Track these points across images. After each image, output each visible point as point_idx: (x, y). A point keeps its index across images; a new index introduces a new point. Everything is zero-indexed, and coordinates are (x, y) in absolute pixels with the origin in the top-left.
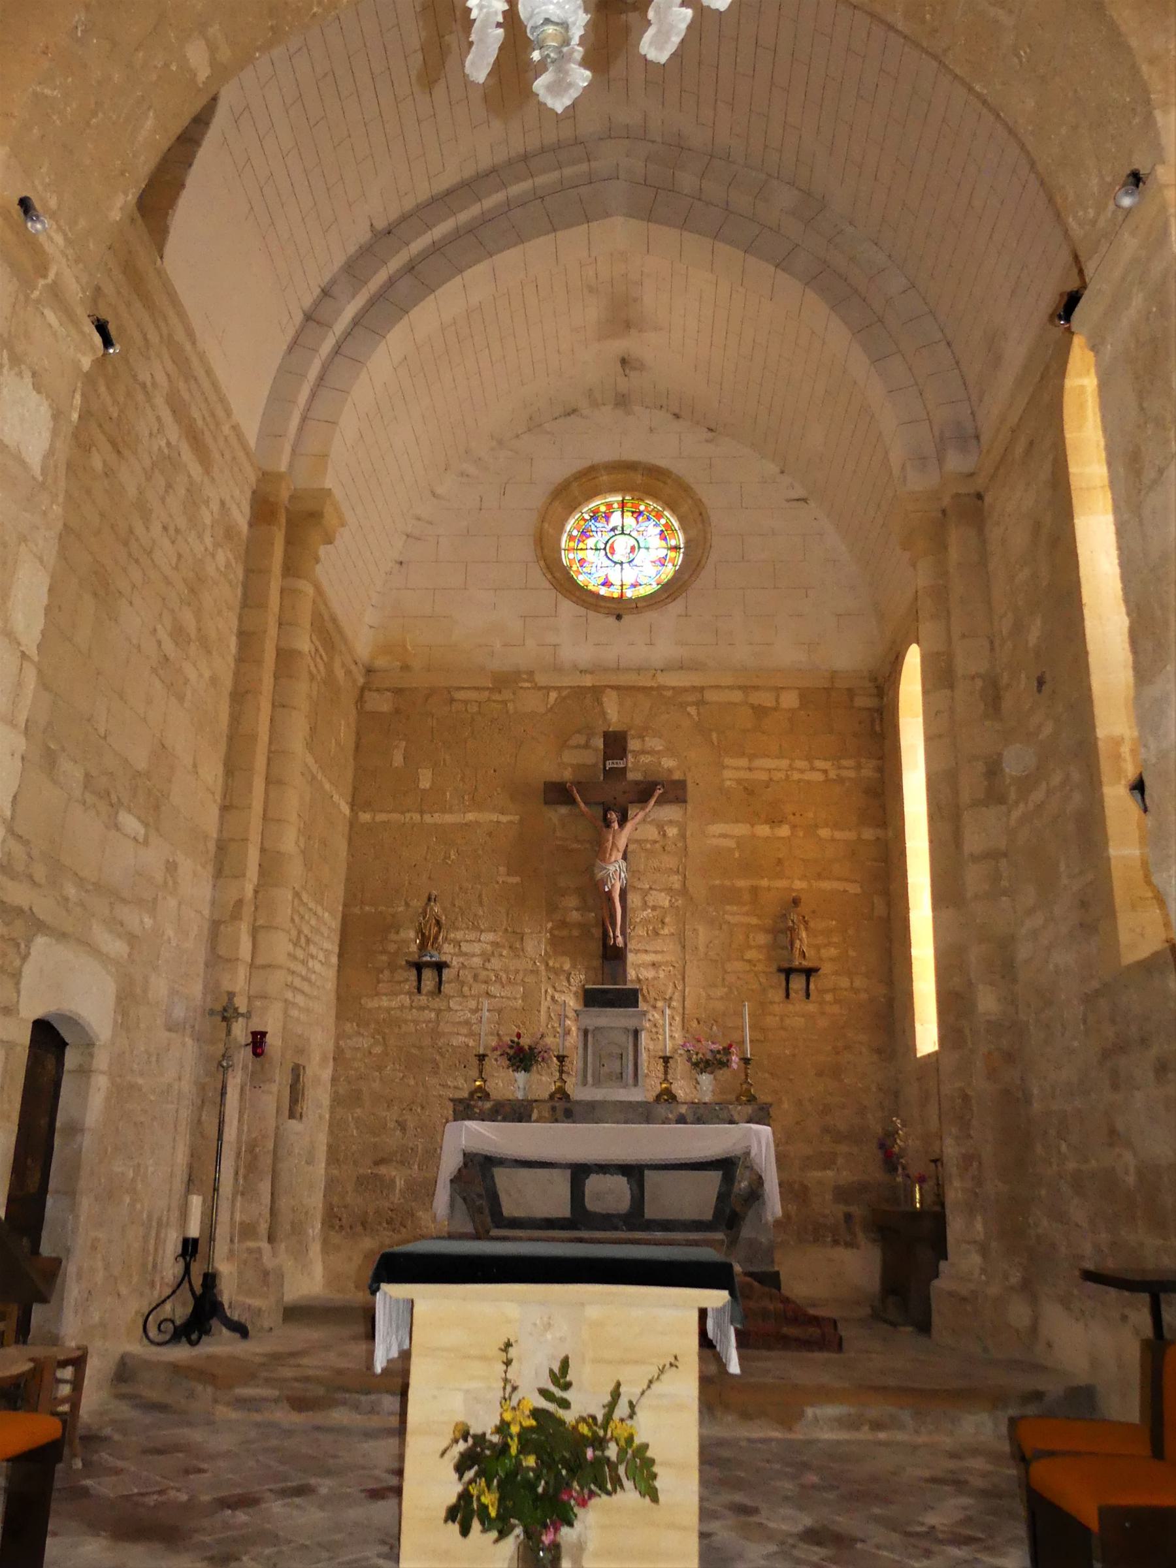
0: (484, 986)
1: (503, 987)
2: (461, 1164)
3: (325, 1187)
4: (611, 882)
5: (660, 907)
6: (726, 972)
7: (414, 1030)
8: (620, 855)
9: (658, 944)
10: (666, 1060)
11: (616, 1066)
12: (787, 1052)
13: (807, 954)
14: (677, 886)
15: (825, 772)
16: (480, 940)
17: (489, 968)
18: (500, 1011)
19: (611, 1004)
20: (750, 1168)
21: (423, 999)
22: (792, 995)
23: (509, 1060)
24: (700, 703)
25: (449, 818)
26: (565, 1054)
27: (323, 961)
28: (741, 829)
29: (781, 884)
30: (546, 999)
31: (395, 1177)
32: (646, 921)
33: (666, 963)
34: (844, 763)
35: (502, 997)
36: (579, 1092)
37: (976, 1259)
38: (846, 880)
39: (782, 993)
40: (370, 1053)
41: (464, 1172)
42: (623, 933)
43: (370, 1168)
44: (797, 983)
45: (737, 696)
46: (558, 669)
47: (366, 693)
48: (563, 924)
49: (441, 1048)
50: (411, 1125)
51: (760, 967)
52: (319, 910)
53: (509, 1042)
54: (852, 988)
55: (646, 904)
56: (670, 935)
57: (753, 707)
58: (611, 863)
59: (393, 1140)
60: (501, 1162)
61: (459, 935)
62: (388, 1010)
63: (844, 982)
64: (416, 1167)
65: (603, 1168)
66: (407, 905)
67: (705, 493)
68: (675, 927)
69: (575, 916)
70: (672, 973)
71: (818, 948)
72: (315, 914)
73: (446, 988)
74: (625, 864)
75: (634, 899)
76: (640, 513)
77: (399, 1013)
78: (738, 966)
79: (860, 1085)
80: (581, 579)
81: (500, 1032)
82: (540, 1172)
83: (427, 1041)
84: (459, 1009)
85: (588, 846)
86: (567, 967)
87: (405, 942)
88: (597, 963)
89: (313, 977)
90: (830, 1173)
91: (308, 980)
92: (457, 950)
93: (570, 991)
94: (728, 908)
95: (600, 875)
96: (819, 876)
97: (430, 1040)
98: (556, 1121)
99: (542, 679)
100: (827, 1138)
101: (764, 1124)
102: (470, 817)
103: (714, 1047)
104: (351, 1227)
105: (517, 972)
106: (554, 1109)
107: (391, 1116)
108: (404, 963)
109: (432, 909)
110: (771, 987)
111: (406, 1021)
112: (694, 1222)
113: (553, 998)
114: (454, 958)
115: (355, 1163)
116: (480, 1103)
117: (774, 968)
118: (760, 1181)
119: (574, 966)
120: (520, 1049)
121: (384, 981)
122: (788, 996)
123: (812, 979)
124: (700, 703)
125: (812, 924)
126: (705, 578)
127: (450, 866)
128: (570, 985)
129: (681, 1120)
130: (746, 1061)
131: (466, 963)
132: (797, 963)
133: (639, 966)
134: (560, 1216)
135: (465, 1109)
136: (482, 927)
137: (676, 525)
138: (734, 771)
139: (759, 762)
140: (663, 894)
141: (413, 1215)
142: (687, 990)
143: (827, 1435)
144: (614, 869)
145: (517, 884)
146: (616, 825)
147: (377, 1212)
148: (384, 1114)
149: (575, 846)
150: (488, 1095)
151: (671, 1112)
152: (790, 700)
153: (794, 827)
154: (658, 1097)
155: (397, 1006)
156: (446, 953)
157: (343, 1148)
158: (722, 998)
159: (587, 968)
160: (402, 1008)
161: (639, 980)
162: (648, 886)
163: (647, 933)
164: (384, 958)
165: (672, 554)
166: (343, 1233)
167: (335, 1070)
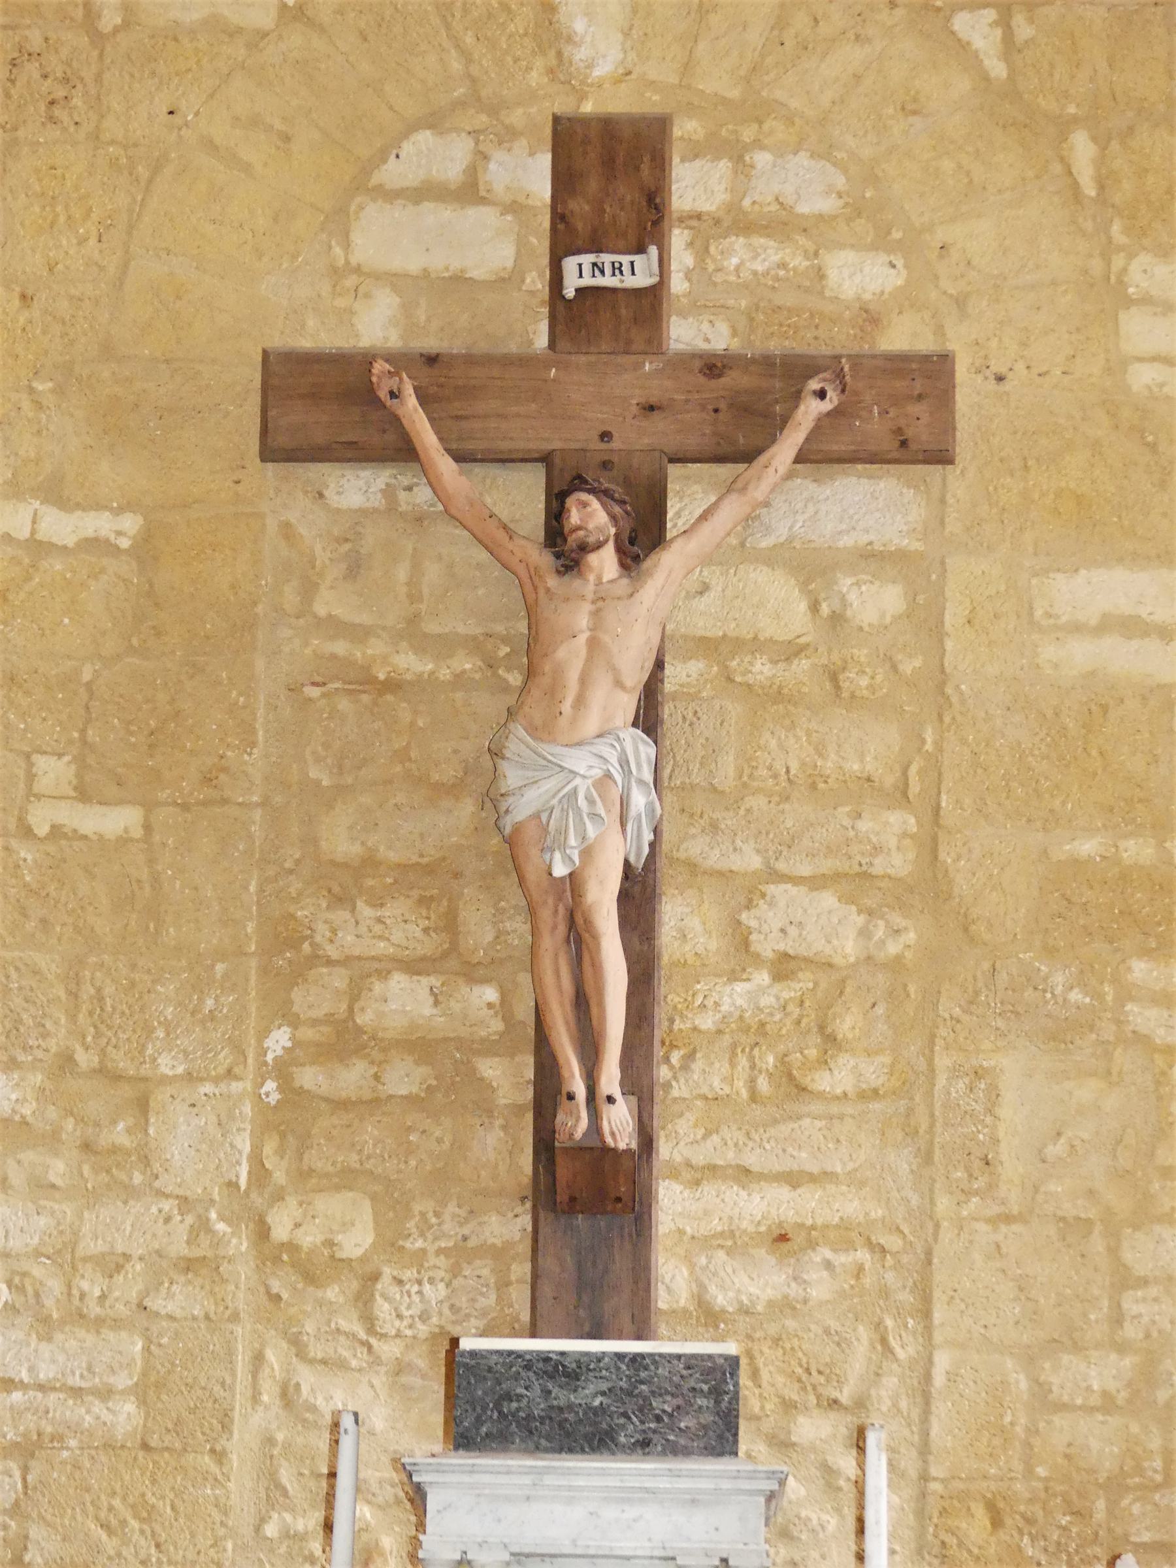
8: (627, 704)
30: (255, 1398)
53: (293, 1383)
55: (746, 943)
85: (466, 664)
93: (377, 1361)
128: (371, 1330)
142: (942, 1361)
145: (124, 841)
146: (605, 562)
149: (409, 663)
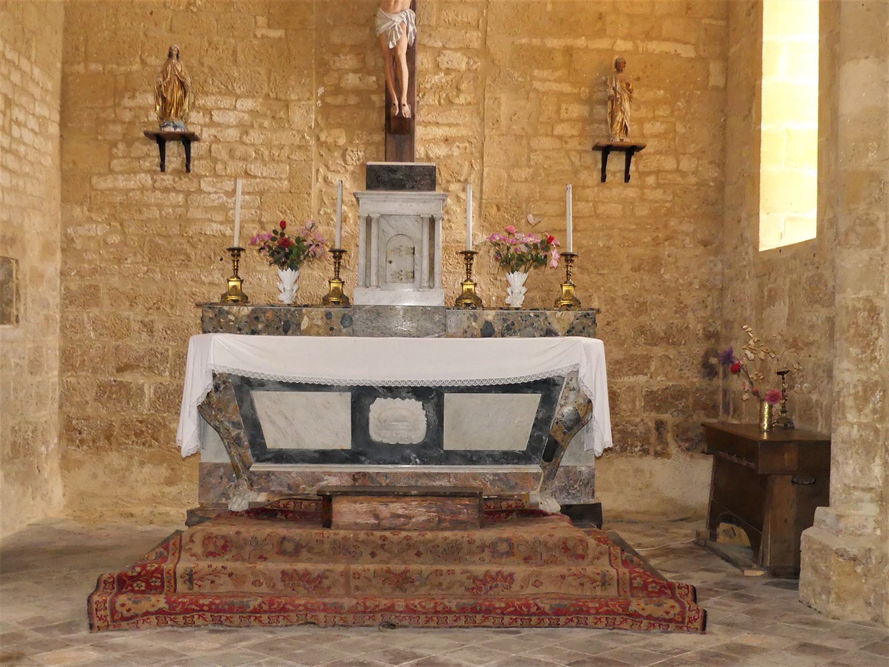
0: (241, 164)
1: (265, 165)
2: (211, 387)
3: (61, 397)
4: (397, 37)
5: (454, 70)
6: (531, 150)
7: (158, 216)
9: (453, 116)
11: (404, 263)
12: (601, 244)
13: (629, 128)
14: (476, 45)
16: (235, 108)
17: (248, 142)
18: (261, 193)
20: (577, 390)
21: (167, 179)
23: (272, 255)
26: (343, 248)
27: (37, 130)
29: (603, 44)
31: (143, 385)
33: (462, 139)
35: (264, 178)
37: (871, 510)
38: (677, 41)
39: (597, 175)
40: (105, 243)
41: (215, 397)
42: (411, 101)
43: (112, 375)
44: (616, 162)
48: (337, 90)
49: (192, 237)
50: (159, 326)
51: (573, 144)
52: (25, 64)
54: (678, 171)
56: (467, 104)
58: (396, 13)
59: (138, 343)
60: (261, 384)
61: (209, 101)
62: (126, 191)
63: (669, 164)
64: (167, 374)
65: (392, 391)
66: (143, 62)
68: (473, 95)
69: (352, 80)
70: (468, 150)
71: (641, 122)
72: (18, 68)
73: (195, 165)
74: (413, 15)
75: (423, 60)
77: (138, 195)
78: (546, 143)
79: (681, 281)
81: (263, 219)
83: (176, 230)
86: (342, 141)
87: (145, 109)
88: (379, 137)
89: (22, 149)
90: (642, 379)
91: (15, 153)
92: (207, 120)
93: (346, 170)
94: (536, 72)
95: (383, 27)
96: (648, 36)
97: (178, 228)
100: (641, 340)
101: (589, 335)
103: (531, 240)
104: (94, 441)
105: (281, 147)
107: (134, 315)
108: (142, 135)
109: (174, 67)
110: (586, 168)
111: (148, 206)
112: (505, 453)
113: (325, 179)
114: (204, 129)
115: (95, 371)
116: (235, 309)
117: (589, 146)
119: (350, 141)
120: (285, 243)
121: (118, 158)
122: (604, 178)
123: (633, 159)
125: (635, 94)
127: (196, 13)
129: (487, 331)
130: (568, 258)
131: (219, 136)
132: (618, 140)
133: (429, 141)
134: (337, 447)
136: (238, 92)
140: (459, 54)
141: (165, 426)
142: (486, 170)
144: (400, 21)
145: (280, 39)
147: (125, 424)
148: (126, 314)
151: (476, 319)
155: (136, 187)
156: (194, 124)
157: (79, 352)
158: (526, 180)
159: (367, 144)
160: (143, 189)
161: (429, 159)
162: (440, 45)
163: (440, 103)
164: (119, 128)
166: (85, 447)
167: (64, 263)
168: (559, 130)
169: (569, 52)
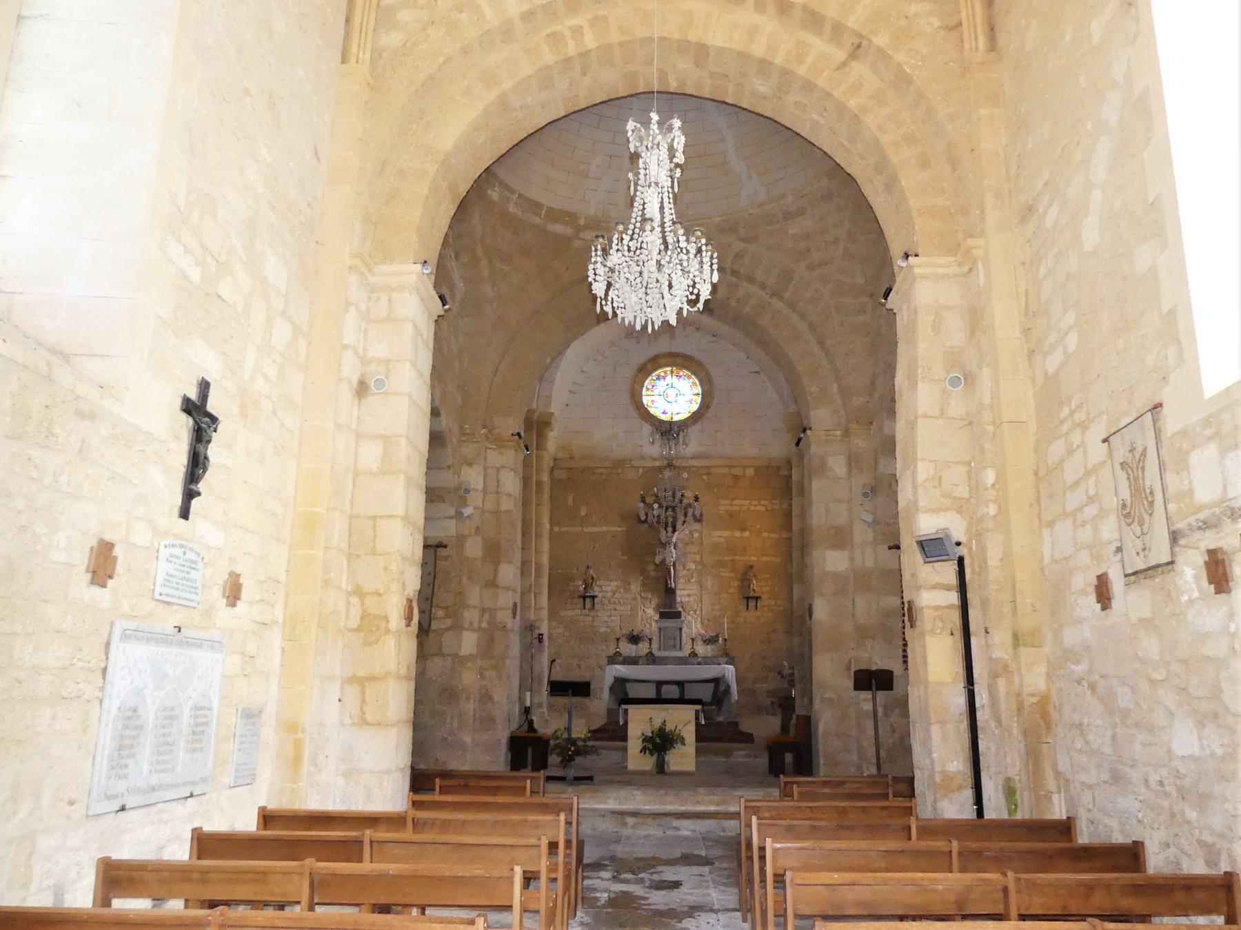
10: (693, 640)
11: (672, 642)
14: (698, 559)
15: (766, 506)
19: (669, 618)
21: (586, 612)
22: (750, 608)
24: (709, 474)
25: (595, 529)
28: (727, 534)
32: (684, 576)
34: (775, 501)
36: (657, 653)
45: (726, 471)
46: (642, 458)
47: (554, 470)
48: (648, 578)
50: (583, 667)
57: (732, 475)
60: (628, 681)
61: (601, 582)
66: (578, 569)
67: (710, 368)
73: (597, 606)
76: (680, 377)
78: (724, 596)
80: (652, 411)
82: (646, 684)
84: (603, 615)
87: (578, 586)
88: (663, 595)
90: (765, 685)
94: (721, 569)
98: (649, 664)
99: (635, 463)
102: (604, 528)
106: (648, 660)
118: (729, 687)
122: (748, 608)
124: (709, 474)
125: (759, 577)
126: (711, 412)
129: (699, 664)
130: (725, 640)
135: (614, 659)
137: (698, 383)
138: (724, 506)
139: (737, 502)
143: (740, 760)
150: (621, 654)
152: (750, 472)
153: (751, 532)
154: (690, 655)
165: (696, 397)
168: (730, 591)
169: (733, 561)
